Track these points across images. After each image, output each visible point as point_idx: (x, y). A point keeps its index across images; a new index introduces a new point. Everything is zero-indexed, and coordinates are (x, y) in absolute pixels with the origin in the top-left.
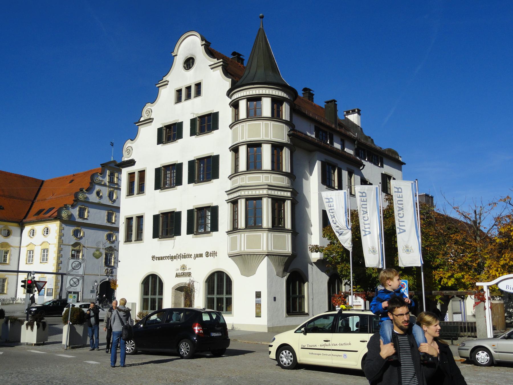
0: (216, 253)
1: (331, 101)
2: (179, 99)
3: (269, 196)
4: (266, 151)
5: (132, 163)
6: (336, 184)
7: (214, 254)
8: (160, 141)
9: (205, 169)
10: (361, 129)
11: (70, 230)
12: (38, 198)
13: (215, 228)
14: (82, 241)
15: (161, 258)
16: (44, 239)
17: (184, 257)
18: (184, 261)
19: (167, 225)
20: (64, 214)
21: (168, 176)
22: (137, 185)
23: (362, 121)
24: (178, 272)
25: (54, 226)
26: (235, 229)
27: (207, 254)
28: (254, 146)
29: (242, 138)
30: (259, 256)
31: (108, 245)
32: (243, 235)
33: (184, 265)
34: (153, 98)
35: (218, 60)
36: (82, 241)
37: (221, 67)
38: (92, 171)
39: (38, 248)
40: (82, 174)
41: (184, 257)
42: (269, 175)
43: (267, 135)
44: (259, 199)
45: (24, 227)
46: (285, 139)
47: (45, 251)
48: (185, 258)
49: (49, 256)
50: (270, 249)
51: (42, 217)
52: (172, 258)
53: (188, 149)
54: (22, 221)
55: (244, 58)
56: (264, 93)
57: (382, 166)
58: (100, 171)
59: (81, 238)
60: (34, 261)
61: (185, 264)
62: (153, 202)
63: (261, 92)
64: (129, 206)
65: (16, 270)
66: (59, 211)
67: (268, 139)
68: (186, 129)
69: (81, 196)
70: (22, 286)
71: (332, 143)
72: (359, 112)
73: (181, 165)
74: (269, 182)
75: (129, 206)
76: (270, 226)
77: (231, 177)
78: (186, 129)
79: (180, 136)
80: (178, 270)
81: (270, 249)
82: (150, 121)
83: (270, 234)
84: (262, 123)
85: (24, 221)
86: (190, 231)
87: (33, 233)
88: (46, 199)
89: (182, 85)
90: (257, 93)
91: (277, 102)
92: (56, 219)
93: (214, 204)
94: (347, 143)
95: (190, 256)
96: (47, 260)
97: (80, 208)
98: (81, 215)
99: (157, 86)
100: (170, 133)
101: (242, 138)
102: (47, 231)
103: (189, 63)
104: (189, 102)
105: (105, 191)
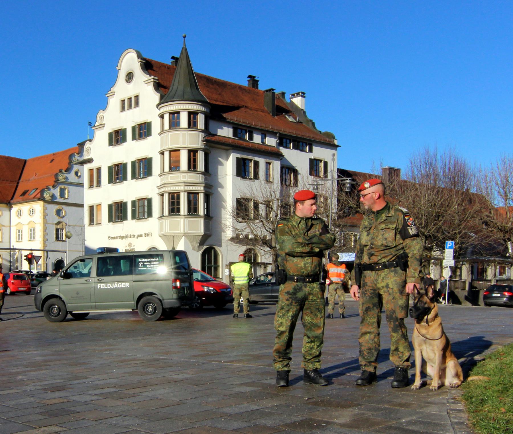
1: (270, 90)
2: (123, 109)
3: (185, 191)
5: (90, 161)
6: (252, 175)
7: (150, 235)
8: (111, 144)
9: (143, 168)
10: (304, 112)
11: (55, 208)
12: (22, 178)
13: (150, 215)
14: (64, 220)
15: (114, 238)
16: (30, 219)
17: (130, 237)
18: (130, 240)
20: (47, 196)
21: (118, 173)
22: (95, 179)
23: (306, 104)
25: (38, 206)
26: (162, 216)
27: (146, 235)
28: (175, 152)
29: (166, 146)
32: (167, 221)
33: (130, 243)
34: (104, 106)
35: (150, 76)
36: (64, 220)
37: (152, 83)
38: (69, 150)
39: (23, 230)
40: (61, 153)
42: (186, 175)
43: (184, 143)
45: (12, 207)
47: (32, 231)
49: (36, 234)
50: (186, 231)
51: (26, 197)
52: (122, 238)
53: (130, 151)
54: (9, 203)
56: (182, 108)
57: (311, 151)
58: (77, 151)
59: (63, 217)
60: (23, 240)
62: (107, 194)
63: (179, 108)
65: (9, 247)
66: (42, 192)
67: (185, 146)
68: (129, 134)
69: (61, 178)
70: (25, 259)
71: (251, 138)
72: (303, 95)
74: (185, 180)
76: (186, 213)
77: (160, 176)
78: (129, 134)
79: (124, 140)
81: (186, 231)
82: (102, 126)
83: (186, 220)
85: (12, 201)
86: (134, 217)
87: (20, 213)
88: (29, 179)
89: (125, 97)
90: (177, 108)
91: (192, 115)
92: (39, 199)
93: (150, 197)
96: (34, 238)
97: (61, 189)
98: (62, 195)
99: (107, 96)
100: (117, 137)
101: (166, 146)
102: (32, 211)
103: (130, 77)
104: (130, 111)
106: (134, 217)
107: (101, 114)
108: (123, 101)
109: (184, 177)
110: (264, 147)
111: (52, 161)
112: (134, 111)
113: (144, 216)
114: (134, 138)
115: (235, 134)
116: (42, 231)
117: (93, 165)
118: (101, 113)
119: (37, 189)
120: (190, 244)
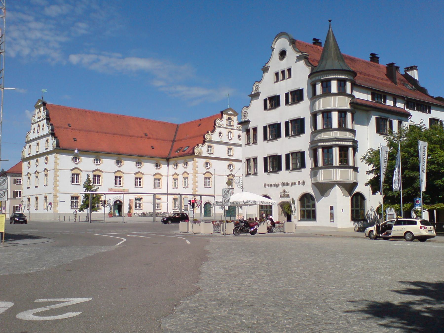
4: (335, 116)
7: (303, 183)
9: (297, 126)
17: (285, 184)
31: (228, 173)
33: (284, 190)
41: (285, 184)
43: (335, 105)
44: (331, 147)
46: (348, 107)
48: (285, 185)
50: (338, 179)
52: (277, 185)
53: (284, 114)
55: (321, 41)
57: (430, 112)
68: (283, 100)
71: (385, 102)
73: (279, 125)
78: (283, 100)
81: (338, 179)
84: (332, 98)
89: (279, 70)
94: (398, 100)
95: (288, 184)
97: (208, 147)
100: (273, 102)
101: (335, 105)
103: (283, 54)
105: (225, 132)
110: (395, 109)
115: (373, 99)
119: (189, 147)
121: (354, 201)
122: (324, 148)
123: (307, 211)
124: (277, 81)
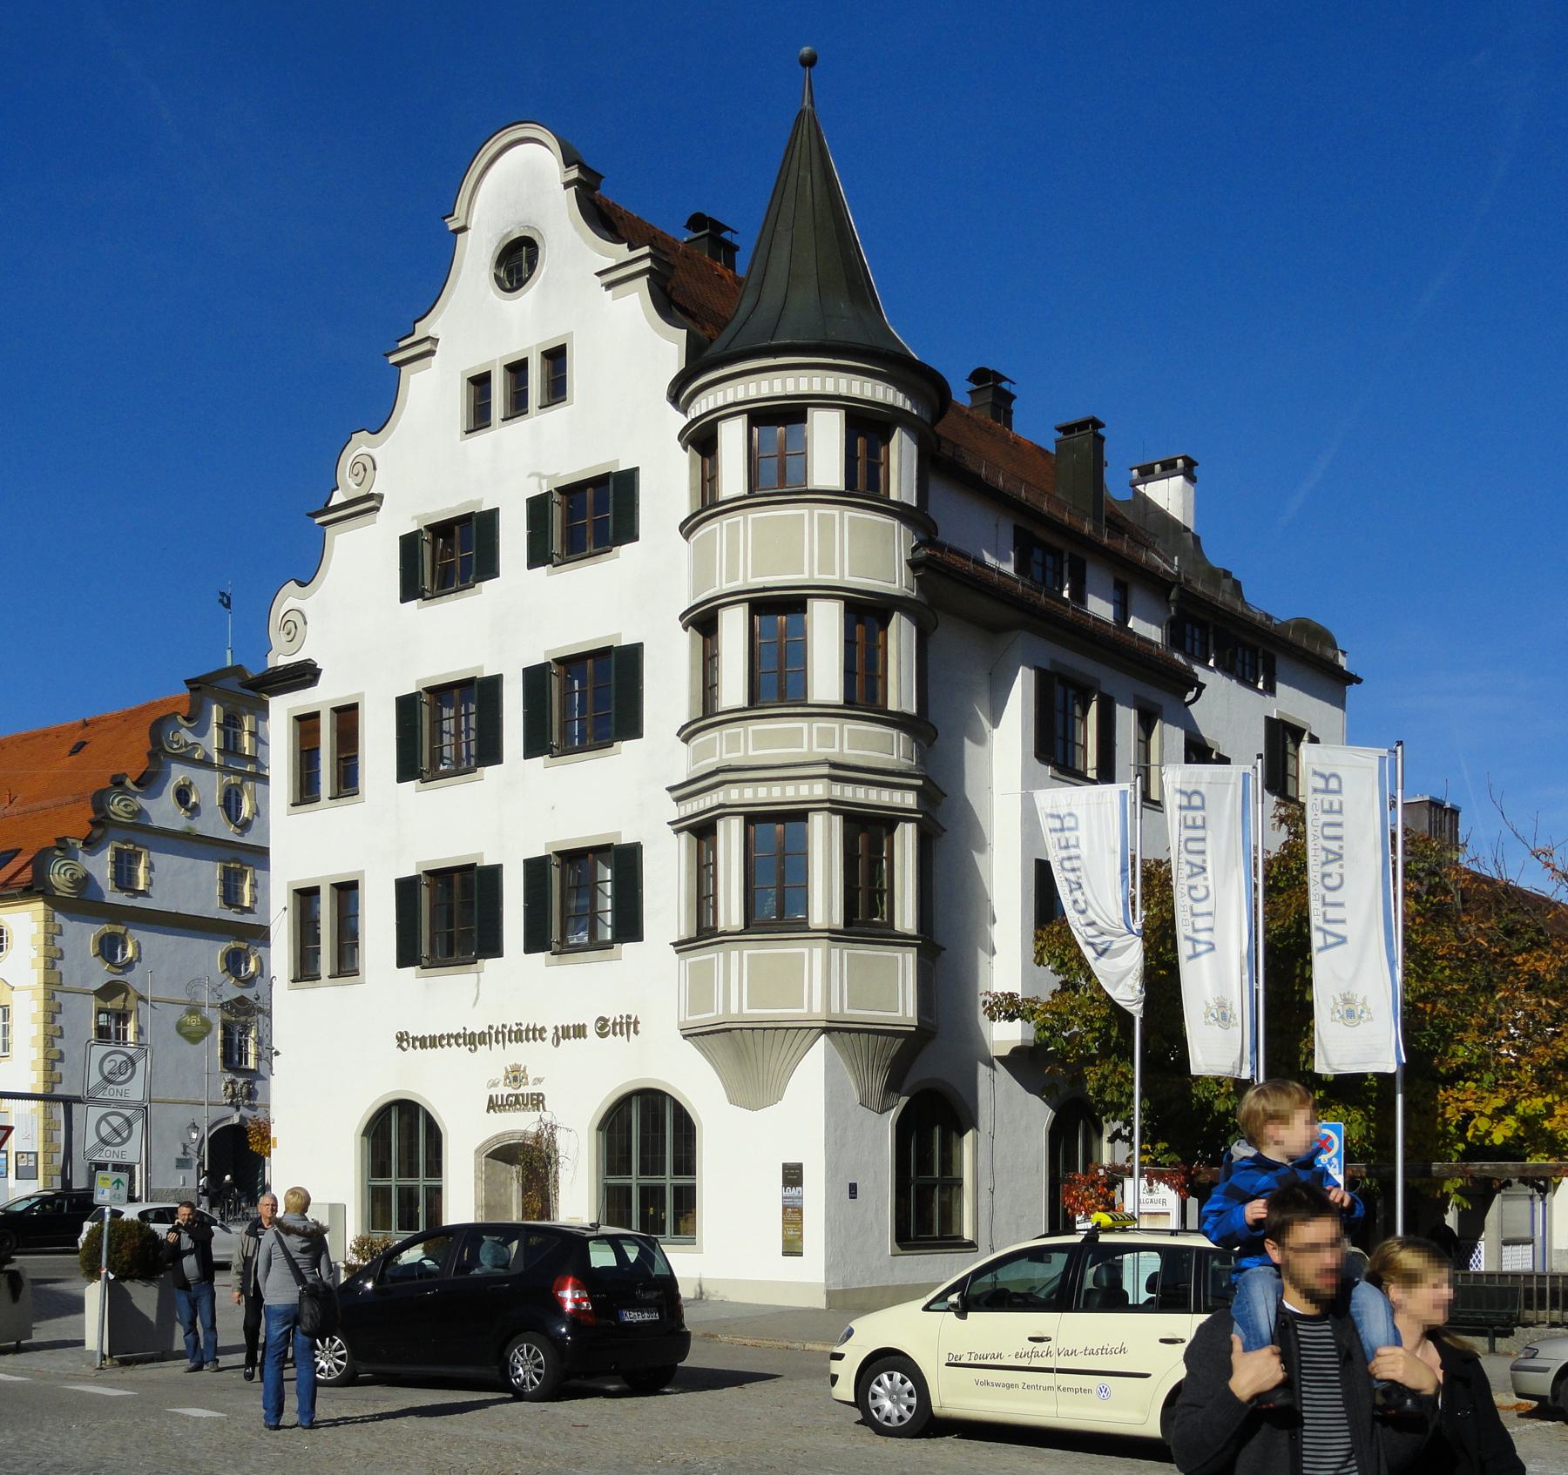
0: (636, 1022)
1: (1082, 425)
2: (479, 418)
4: (825, 628)
5: (305, 675)
7: (628, 1026)
8: (411, 589)
9: (590, 699)
10: (1196, 539)
13: (629, 927)
14: (131, 978)
17: (518, 1035)
18: (517, 1053)
19: (450, 916)
20: (59, 876)
21: (448, 728)
22: (329, 760)
24: (494, 1092)
26: (704, 933)
28: (777, 609)
29: (732, 576)
30: (795, 1034)
31: (232, 991)
32: (734, 954)
34: (377, 409)
36: (131, 978)
41: (518, 1035)
43: (826, 565)
46: (896, 580)
48: (519, 1039)
50: (835, 1009)
52: (474, 1040)
53: (523, 618)
55: (736, 240)
56: (817, 388)
57: (1270, 690)
58: (185, 709)
59: (128, 966)
61: (522, 1063)
62: (388, 832)
63: (804, 388)
64: (306, 845)
66: (40, 863)
67: (833, 579)
69: (117, 807)
71: (1079, 596)
72: (1189, 473)
73: (495, 683)
74: (833, 752)
75: (306, 845)
76: (838, 921)
77: (688, 733)
79: (487, 567)
80: (495, 1085)
81: (835, 1009)
82: (368, 504)
83: (835, 952)
86: (536, 940)
89: (493, 356)
90: (791, 389)
91: (867, 428)
94: (1137, 597)
95: (537, 1033)
98: (124, 879)
99: (393, 359)
100: (448, 556)
101: (732, 576)
103: (517, 261)
104: (521, 425)
105: (209, 787)
106: (536, 940)
107: (363, 449)
108: (480, 382)
109: (826, 736)
111: (79, 747)
112: (541, 423)
113: (593, 934)
114: (538, 555)
116: (41, 1017)
117: (319, 698)
118: (360, 445)
120: (853, 1084)
121: (379, 1213)
122: (754, 818)
123: (400, 1189)
124: (479, 418)
